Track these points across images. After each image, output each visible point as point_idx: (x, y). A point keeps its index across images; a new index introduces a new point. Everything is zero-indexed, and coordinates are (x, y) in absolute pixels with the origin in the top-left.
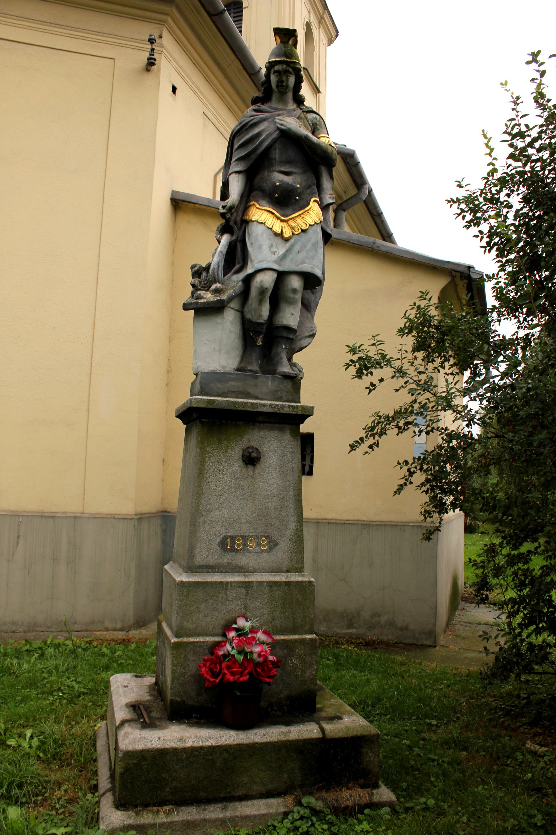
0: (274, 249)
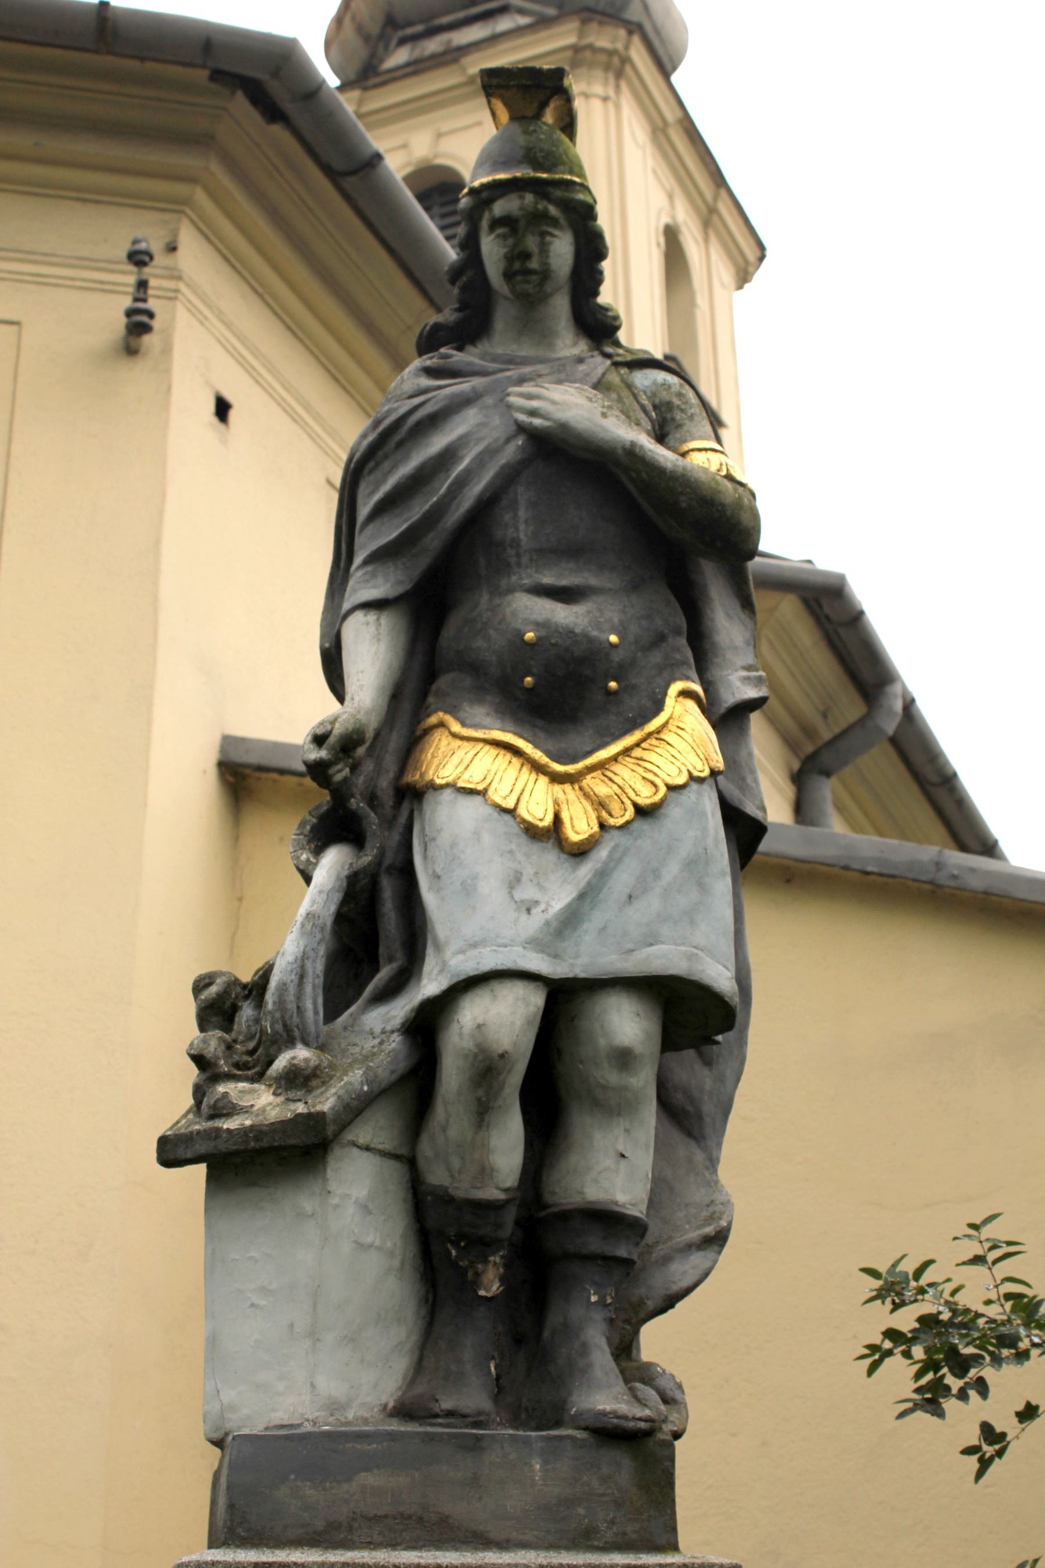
0: (527, 892)
